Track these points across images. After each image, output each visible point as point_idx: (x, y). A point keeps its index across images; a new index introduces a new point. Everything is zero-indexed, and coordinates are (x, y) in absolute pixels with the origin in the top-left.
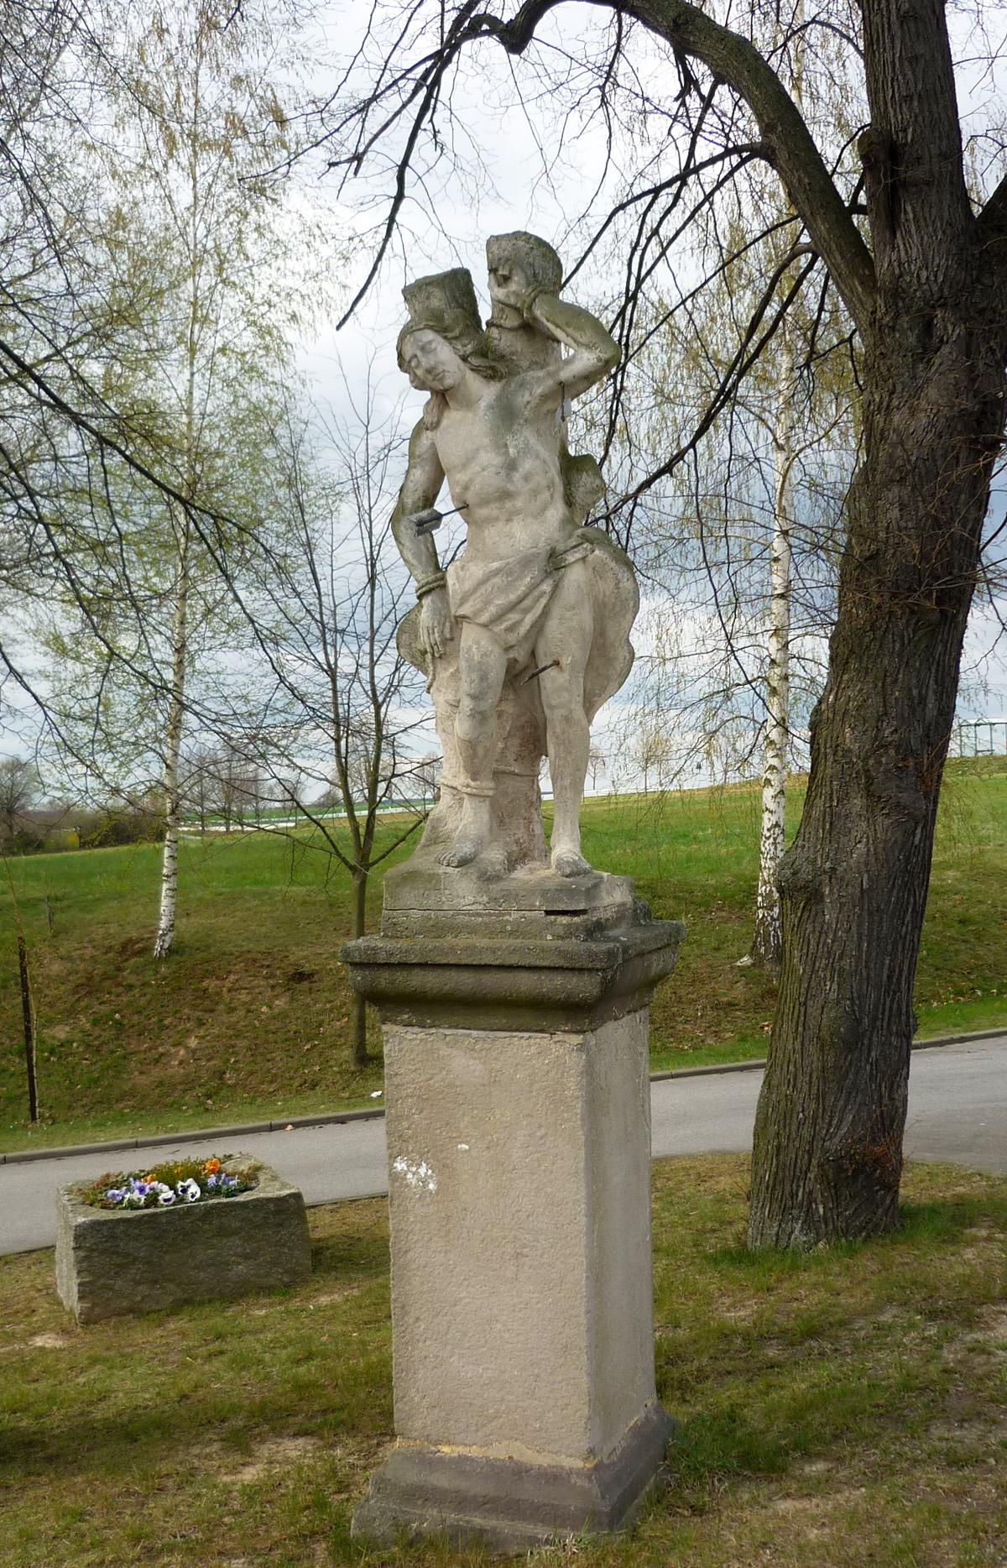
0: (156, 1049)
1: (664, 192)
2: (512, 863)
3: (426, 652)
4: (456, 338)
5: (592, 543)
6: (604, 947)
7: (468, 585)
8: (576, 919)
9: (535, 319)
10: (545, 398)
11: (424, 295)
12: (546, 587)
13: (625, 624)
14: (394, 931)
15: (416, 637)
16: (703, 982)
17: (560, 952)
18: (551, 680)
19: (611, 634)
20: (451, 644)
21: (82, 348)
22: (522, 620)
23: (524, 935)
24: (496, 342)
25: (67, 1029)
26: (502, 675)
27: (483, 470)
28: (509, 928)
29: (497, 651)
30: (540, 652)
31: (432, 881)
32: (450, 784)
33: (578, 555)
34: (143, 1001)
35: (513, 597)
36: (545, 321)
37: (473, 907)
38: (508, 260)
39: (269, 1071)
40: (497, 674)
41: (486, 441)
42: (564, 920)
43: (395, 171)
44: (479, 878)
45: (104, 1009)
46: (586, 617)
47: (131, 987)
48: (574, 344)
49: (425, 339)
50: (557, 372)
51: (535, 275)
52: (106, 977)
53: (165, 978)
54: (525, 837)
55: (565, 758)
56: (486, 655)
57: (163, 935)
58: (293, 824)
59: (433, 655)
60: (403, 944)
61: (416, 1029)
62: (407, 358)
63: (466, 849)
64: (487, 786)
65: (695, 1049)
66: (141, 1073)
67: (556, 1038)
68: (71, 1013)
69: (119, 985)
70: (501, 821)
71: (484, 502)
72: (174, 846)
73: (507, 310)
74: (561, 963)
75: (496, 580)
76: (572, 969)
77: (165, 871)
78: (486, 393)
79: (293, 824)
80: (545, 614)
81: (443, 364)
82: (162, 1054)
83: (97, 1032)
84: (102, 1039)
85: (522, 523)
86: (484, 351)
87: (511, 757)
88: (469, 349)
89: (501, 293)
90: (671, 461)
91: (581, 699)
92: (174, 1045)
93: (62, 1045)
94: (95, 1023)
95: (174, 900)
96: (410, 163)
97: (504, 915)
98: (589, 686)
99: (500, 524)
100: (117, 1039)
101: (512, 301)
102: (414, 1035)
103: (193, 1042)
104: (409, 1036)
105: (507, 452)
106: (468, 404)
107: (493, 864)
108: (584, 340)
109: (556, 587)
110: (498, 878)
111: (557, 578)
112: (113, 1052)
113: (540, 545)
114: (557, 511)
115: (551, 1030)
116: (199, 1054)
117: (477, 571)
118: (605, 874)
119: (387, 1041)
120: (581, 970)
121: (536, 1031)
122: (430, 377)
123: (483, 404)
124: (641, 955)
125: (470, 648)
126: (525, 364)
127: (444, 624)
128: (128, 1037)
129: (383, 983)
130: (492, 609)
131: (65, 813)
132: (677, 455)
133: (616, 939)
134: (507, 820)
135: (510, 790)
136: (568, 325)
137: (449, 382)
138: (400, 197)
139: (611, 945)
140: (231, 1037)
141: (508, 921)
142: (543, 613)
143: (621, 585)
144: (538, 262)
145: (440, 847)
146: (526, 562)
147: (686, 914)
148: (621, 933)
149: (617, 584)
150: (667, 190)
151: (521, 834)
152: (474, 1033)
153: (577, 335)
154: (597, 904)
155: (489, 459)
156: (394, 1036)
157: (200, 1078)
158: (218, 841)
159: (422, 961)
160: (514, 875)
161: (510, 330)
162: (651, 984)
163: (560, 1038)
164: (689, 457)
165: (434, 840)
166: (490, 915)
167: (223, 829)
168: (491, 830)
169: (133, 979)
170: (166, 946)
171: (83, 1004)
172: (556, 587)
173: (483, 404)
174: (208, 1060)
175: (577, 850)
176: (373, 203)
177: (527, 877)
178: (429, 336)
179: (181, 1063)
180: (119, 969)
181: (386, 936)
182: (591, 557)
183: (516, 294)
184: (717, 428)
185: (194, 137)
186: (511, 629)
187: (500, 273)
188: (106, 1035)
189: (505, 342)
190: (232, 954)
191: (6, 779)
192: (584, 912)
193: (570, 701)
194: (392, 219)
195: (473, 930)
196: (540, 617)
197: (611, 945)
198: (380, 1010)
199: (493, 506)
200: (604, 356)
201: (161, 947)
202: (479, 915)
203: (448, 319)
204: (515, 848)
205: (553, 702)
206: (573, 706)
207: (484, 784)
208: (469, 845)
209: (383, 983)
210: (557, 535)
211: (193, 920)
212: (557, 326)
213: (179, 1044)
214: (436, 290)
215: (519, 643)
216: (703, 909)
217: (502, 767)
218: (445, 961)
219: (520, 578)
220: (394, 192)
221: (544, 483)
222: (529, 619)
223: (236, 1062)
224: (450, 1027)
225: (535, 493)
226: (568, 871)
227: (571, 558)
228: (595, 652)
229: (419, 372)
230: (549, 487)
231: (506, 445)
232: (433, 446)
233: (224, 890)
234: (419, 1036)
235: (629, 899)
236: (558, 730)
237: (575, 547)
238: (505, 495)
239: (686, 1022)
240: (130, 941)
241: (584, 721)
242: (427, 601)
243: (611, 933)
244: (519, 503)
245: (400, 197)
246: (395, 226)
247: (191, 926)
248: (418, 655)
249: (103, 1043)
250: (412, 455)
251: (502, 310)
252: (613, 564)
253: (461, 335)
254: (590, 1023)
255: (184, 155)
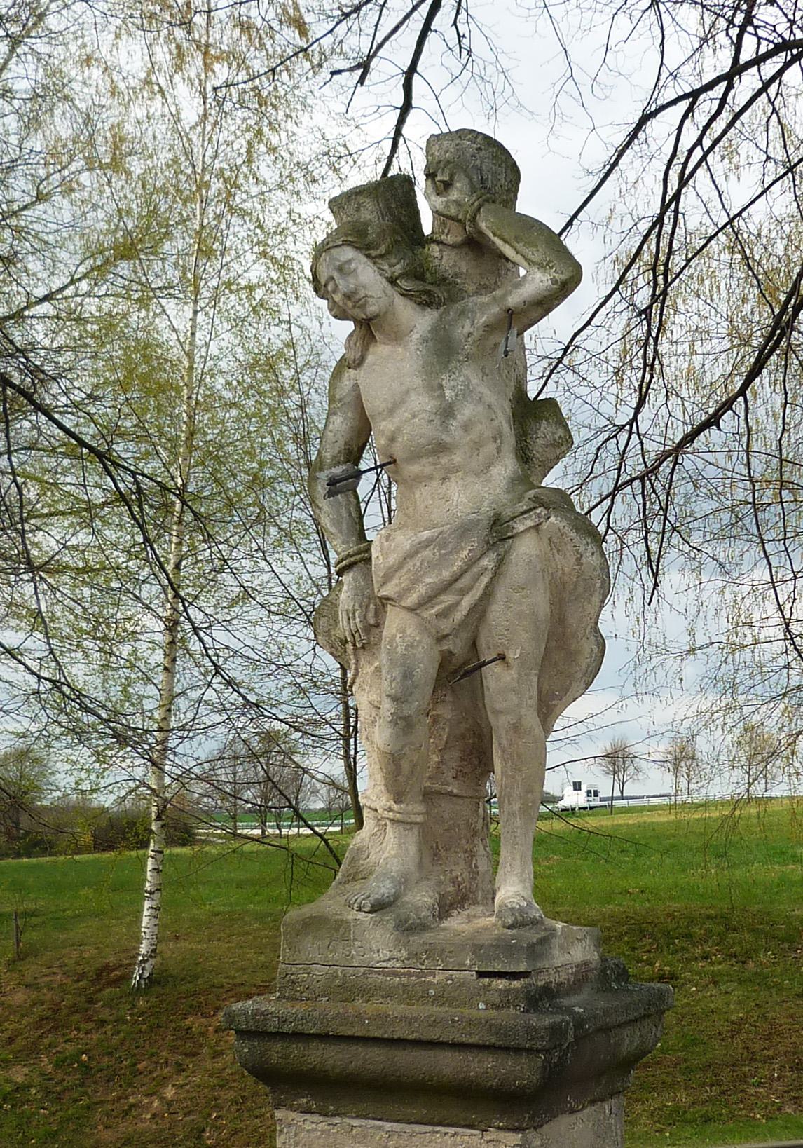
0: (126, 1098)
1: (702, 97)
2: (445, 908)
3: (347, 642)
4: (381, 256)
5: (547, 508)
6: (548, 1021)
7: (393, 559)
8: (516, 984)
9: (481, 233)
10: (490, 328)
11: (353, 205)
12: (488, 562)
13: (591, 610)
14: (292, 991)
15: (336, 622)
16: (781, 1035)
17: (490, 1025)
18: (495, 677)
19: (573, 621)
20: (377, 631)
21: (84, 286)
22: (458, 603)
23: (450, 1002)
24: (437, 262)
25: (26, 1070)
26: (433, 671)
27: (414, 416)
28: (432, 992)
29: (427, 641)
30: (482, 642)
31: (338, 929)
32: (372, 806)
33: (529, 523)
34: (116, 1040)
35: (446, 574)
36: (491, 236)
37: (390, 964)
38: (449, 162)
39: (256, 1130)
40: (426, 669)
41: (418, 381)
42: (501, 984)
43: (401, 80)
44: (397, 927)
45: (70, 1048)
46: (540, 601)
47: (103, 1023)
48: (525, 264)
49: (343, 258)
50: (504, 297)
51: (482, 181)
52: (74, 1009)
53: (142, 1014)
54: (465, 874)
55: (513, 777)
56: (412, 646)
57: (144, 961)
58: (338, 829)
59: (354, 645)
60: (300, 1008)
61: (316, 1118)
62: (323, 281)
63: (383, 890)
64: (415, 809)
65: (768, 1118)
66: (106, 1127)
67: (488, 1137)
68: (33, 1050)
69: (89, 1019)
70: (435, 855)
71: (415, 456)
72: (160, 857)
73: (449, 222)
74: (492, 1039)
75: (427, 553)
76: (506, 1049)
77: (148, 886)
78: (420, 322)
79: (338, 829)
80: (488, 595)
81: (365, 287)
82: (132, 1106)
83: (59, 1076)
84: (65, 1084)
85: (461, 482)
86: (417, 273)
87: (449, 774)
88: (398, 269)
89: (439, 202)
90: (717, 411)
91: (534, 702)
92: (147, 1095)
93: (17, 1090)
94: (58, 1065)
95: (157, 922)
96: (419, 69)
97: (426, 975)
98: (546, 687)
99: (435, 484)
100: (82, 1085)
101: (453, 211)
102: (313, 1126)
103: (169, 1092)
104: (308, 1126)
105: (443, 395)
106: (397, 337)
107: (418, 909)
108: (536, 257)
109: (501, 562)
110: (423, 927)
111: (502, 551)
112: (76, 1101)
113: (483, 510)
114: (506, 467)
115: (482, 1126)
116: (176, 1105)
117: (404, 541)
118: (559, 925)
119: (281, 1131)
120: (518, 1050)
121: (463, 1126)
122: (350, 304)
123: (415, 336)
124: (605, 1030)
125: (394, 637)
126: (470, 288)
127: (367, 607)
128: (95, 1082)
129: (275, 1057)
130: (421, 590)
131: (82, 811)
132: (724, 404)
133: (569, 1010)
134: (443, 853)
135: (446, 816)
136: (517, 239)
137: (372, 309)
138: (406, 107)
139: (558, 1018)
140: (213, 1088)
141: (431, 983)
142: (485, 593)
143: (584, 560)
144: (487, 166)
145: (358, 885)
146: (464, 530)
147: (766, 951)
148: (578, 1003)
149: (578, 560)
150: (711, 94)
151: (460, 871)
152: (388, 1126)
153: (528, 252)
154: (545, 963)
155: (422, 403)
156: (289, 1125)
157: (174, 1136)
158: (249, 847)
159: (322, 1031)
160: (445, 924)
161: (453, 246)
162: (629, 1063)
163: (494, 1137)
164: (739, 405)
165: (353, 877)
166: (409, 975)
167: (259, 832)
168: (420, 865)
169: (105, 1014)
170: (146, 975)
171: (46, 1041)
172: (501, 562)
173: (415, 336)
174: (186, 1115)
175: (528, 893)
176: (377, 115)
177: (460, 928)
178: (348, 253)
179: (154, 1116)
180: (91, 1001)
181: (282, 997)
182: (545, 526)
183: (458, 203)
184: (18, 306)
185: (205, 49)
186: (443, 614)
187: (439, 178)
188: (71, 1080)
189: (444, 260)
190: (222, 987)
191: (12, 772)
192: (525, 974)
193: (519, 705)
194: (398, 133)
195: (388, 993)
196: (481, 599)
197: (558, 1018)
198: (273, 1092)
199: (424, 461)
200: (559, 277)
201: (141, 976)
202: (396, 974)
203: (372, 234)
204: (450, 889)
205: (498, 706)
206: (523, 711)
207: (410, 807)
208: (388, 884)
209: (275, 1057)
210: (504, 497)
211: (182, 944)
212: (505, 242)
213: (154, 1094)
214: (367, 200)
215: (455, 632)
216: (786, 945)
217: (437, 787)
218: (349, 1033)
219: (456, 550)
220: (400, 102)
221: (489, 433)
222: (467, 602)
223: (218, 1117)
224: (357, 1117)
225: (477, 446)
226: (510, 921)
227: (520, 527)
228: (553, 644)
229: (337, 298)
230: (495, 440)
231: (441, 387)
232: (356, 387)
233: (222, 909)
234: (320, 1127)
235: (594, 957)
236: (504, 742)
237: (523, 513)
238: (440, 448)
239: (760, 1085)
240: (106, 967)
241: (538, 730)
242: (347, 578)
243: (566, 1002)
244: (457, 458)
245: (406, 107)
246: (401, 140)
247: (174, 951)
248: (338, 644)
249: (68, 1089)
250: (332, 399)
251: (444, 223)
252: (573, 534)
253: (388, 253)
254: (532, 1118)
255: (194, 67)
